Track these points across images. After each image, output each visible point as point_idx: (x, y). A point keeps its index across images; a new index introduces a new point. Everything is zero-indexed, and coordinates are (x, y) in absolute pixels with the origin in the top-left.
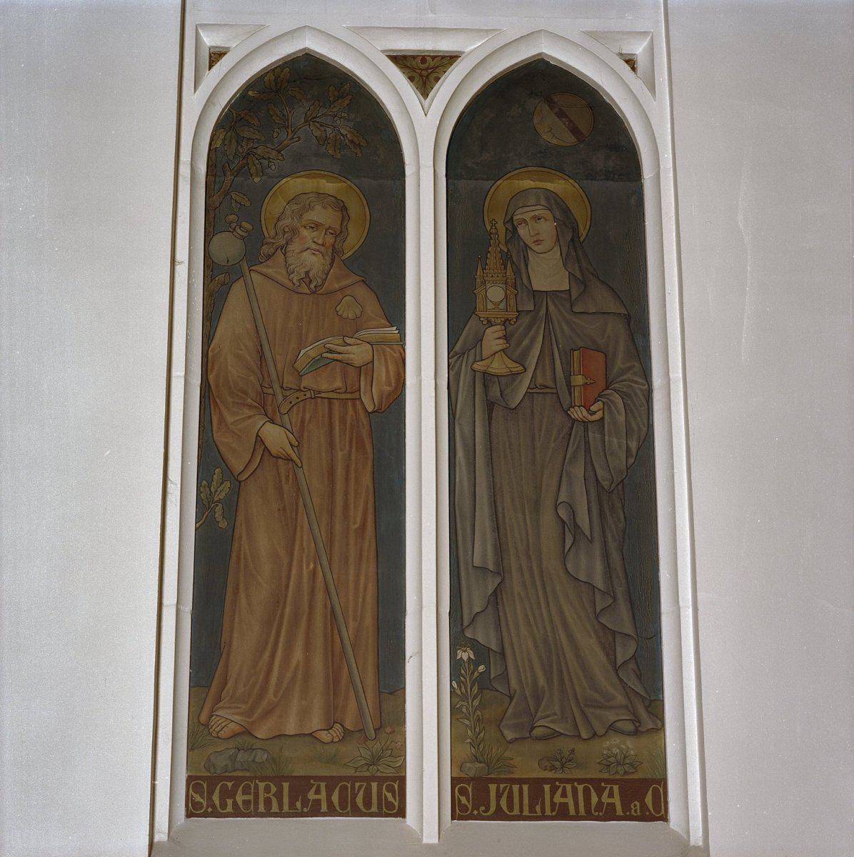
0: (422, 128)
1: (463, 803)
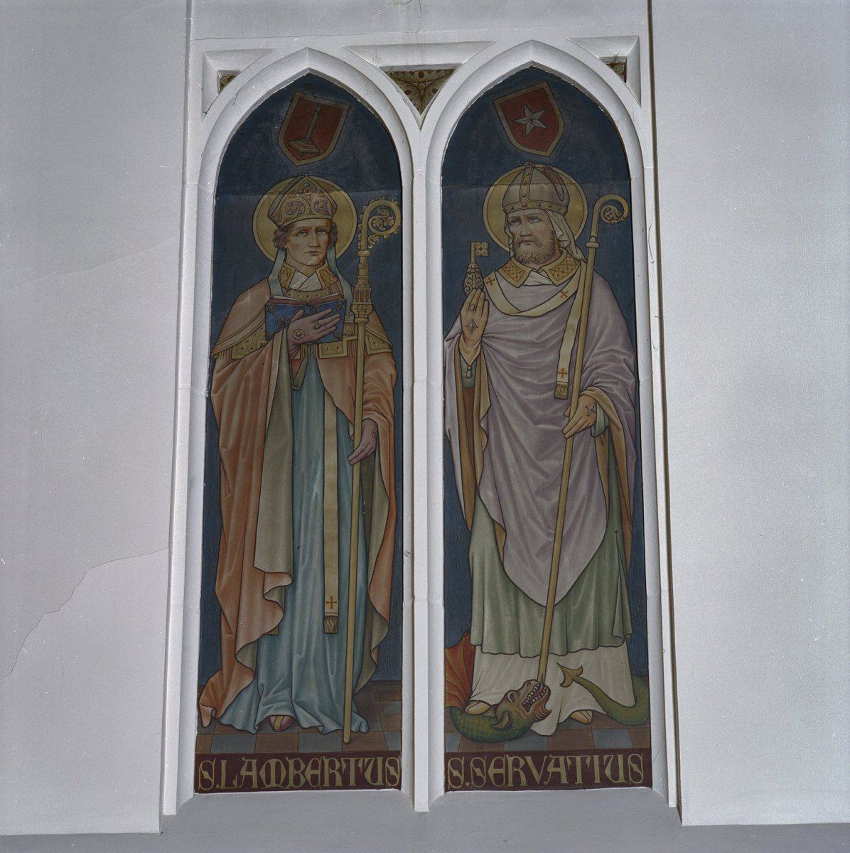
0: (423, 141)
1: (391, 774)
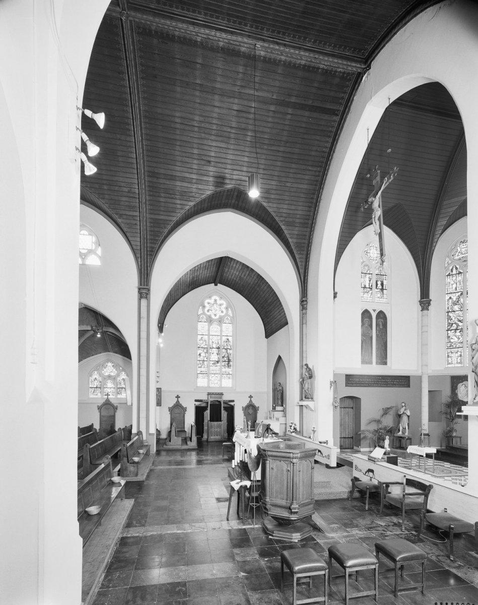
0: (374, 315)
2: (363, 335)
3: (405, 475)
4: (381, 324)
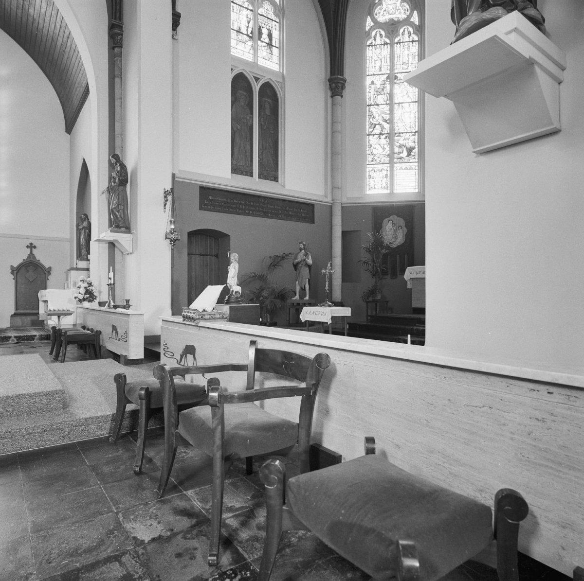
0: (256, 88)
2: (234, 120)
3: (254, 339)
4: (267, 106)
